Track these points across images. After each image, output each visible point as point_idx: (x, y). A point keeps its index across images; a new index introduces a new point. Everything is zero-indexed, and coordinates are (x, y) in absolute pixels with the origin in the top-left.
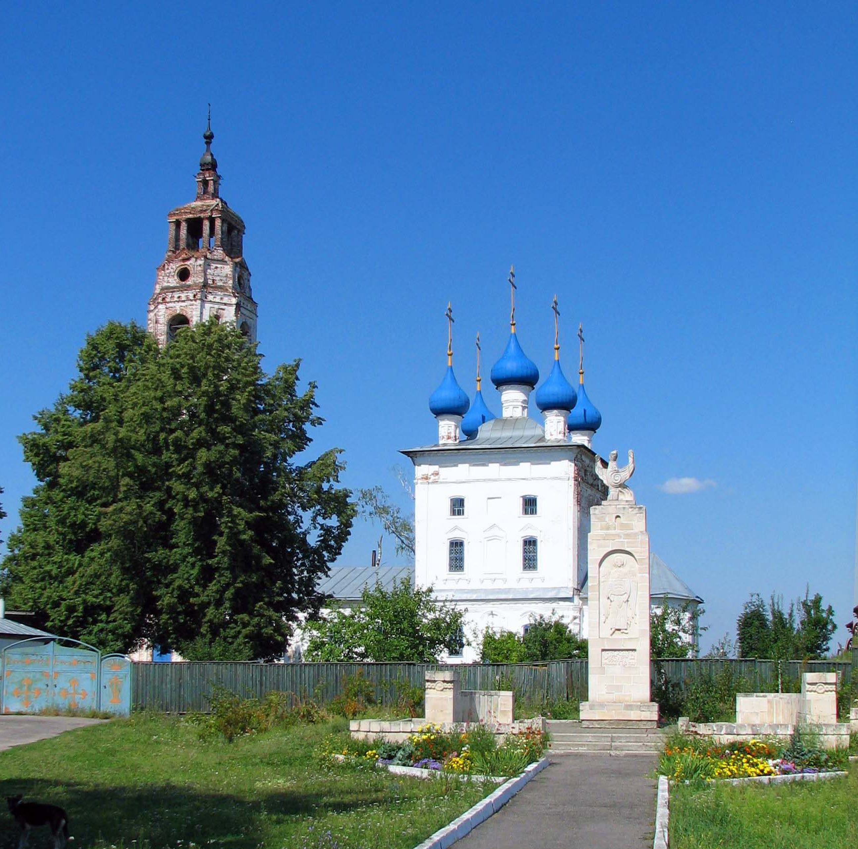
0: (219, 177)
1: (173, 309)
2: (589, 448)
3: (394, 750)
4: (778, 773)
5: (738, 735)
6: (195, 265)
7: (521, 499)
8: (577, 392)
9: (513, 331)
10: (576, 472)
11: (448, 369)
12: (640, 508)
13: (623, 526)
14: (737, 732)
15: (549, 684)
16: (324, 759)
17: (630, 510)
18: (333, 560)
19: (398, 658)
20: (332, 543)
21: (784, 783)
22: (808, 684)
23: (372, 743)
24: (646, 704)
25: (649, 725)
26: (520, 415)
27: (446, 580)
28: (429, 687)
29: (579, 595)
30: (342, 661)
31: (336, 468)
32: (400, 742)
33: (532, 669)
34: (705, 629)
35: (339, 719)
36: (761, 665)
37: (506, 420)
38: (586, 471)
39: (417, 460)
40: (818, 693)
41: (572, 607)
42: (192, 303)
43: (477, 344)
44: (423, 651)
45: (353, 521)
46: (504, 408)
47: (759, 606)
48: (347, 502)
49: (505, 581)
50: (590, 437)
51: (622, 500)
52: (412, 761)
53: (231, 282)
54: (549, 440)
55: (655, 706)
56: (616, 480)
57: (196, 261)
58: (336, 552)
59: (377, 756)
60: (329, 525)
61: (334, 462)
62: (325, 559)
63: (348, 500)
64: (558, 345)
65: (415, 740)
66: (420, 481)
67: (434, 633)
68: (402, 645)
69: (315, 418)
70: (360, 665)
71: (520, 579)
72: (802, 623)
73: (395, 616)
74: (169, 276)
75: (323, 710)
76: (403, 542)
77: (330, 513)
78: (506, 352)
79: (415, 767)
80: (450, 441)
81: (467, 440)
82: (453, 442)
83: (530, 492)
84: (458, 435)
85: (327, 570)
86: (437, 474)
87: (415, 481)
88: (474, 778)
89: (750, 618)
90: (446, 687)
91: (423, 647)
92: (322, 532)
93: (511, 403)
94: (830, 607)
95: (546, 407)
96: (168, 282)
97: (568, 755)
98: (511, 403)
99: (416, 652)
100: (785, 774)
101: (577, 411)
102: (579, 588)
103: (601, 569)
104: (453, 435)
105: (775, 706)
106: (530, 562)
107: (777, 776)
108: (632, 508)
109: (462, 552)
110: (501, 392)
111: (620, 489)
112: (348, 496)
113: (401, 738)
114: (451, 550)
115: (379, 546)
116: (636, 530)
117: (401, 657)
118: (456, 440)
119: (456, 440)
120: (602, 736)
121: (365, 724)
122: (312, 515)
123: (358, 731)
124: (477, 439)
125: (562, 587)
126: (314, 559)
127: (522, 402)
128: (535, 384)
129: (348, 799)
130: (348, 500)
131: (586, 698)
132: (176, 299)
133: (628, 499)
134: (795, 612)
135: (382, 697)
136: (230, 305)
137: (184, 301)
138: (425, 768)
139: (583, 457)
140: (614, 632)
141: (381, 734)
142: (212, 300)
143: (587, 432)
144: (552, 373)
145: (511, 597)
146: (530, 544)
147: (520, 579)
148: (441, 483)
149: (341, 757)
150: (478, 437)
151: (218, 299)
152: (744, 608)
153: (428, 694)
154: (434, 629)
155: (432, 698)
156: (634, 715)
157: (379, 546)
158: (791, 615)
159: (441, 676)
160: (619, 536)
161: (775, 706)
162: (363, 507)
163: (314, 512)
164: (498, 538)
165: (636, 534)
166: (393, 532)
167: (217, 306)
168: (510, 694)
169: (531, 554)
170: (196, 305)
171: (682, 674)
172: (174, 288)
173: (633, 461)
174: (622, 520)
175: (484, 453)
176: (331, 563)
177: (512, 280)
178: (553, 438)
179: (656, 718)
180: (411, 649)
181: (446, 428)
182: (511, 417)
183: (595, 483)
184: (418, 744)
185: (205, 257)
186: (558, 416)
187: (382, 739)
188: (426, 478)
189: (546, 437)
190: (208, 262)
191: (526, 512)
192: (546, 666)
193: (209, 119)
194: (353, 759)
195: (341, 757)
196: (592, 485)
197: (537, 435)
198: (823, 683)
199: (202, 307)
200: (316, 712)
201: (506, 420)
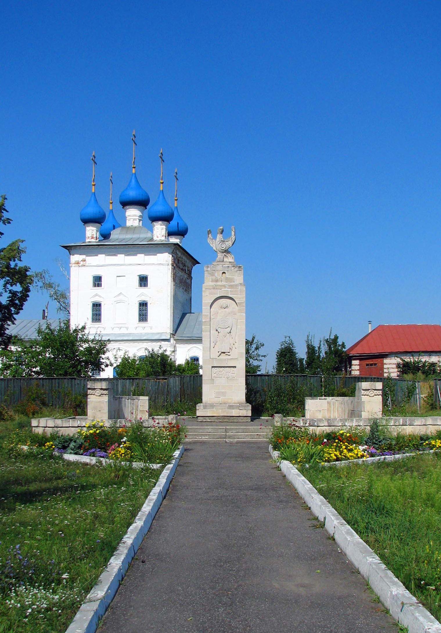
3: (67, 442)
4: (368, 456)
5: (318, 426)
7: (138, 277)
8: (174, 210)
9: (134, 172)
10: (173, 261)
11: (92, 194)
12: (240, 267)
13: (227, 280)
14: (317, 424)
15: (168, 391)
16: (12, 449)
17: (233, 268)
18: (17, 313)
19: (64, 375)
20: (17, 302)
21: (373, 463)
22: (363, 390)
23: (50, 436)
24: (243, 405)
25: (245, 420)
26: (138, 225)
27: (90, 328)
28: (90, 393)
29: (174, 338)
30: (24, 377)
31: (19, 251)
32: (71, 435)
34: (264, 356)
35: (24, 418)
36: (311, 379)
37: (128, 228)
38: (178, 260)
39: (72, 252)
40: (370, 396)
41: (169, 345)
43: (111, 180)
44: (80, 370)
45: (31, 287)
46: (127, 220)
47: (290, 344)
48: (27, 275)
49: (127, 328)
50: (181, 240)
51: (226, 262)
52: (82, 451)
54: (156, 240)
55: (250, 407)
56: (222, 248)
58: (19, 308)
59: (54, 447)
60: (15, 290)
61: (18, 248)
62: (13, 312)
63: (28, 273)
64: (163, 181)
65: (84, 434)
66: (73, 265)
67: (88, 357)
68: (66, 366)
69: (6, 219)
70: (37, 379)
72: (326, 353)
73: (61, 346)
75: (11, 411)
76: (61, 305)
77: (16, 282)
78: (129, 185)
79: (85, 455)
80: (93, 240)
81: (103, 240)
82: (94, 241)
83: (143, 273)
84: (98, 236)
85: (13, 320)
86: (85, 261)
87: (70, 265)
88: (135, 465)
89: (284, 352)
90: (103, 393)
91: (81, 367)
92: (10, 295)
93: (131, 218)
94: (343, 343)
95: (155, 219)
97: (195, 443)
98: (131, 218)
99: (76, 370)
100: (373, 457)
101: (173, 223)
102: (174, 333)
103: (211, 309)
104: (95, 236)
105: (332, 406)
106: (143, 317)
107: (368, 459)
108: (233, 267)
109: (100, 310)
111: (225, 253)
112: (27, 271)
113: (71, 432)
115: (47, 308)
116: (237, 282)
117: (66, 374)
119: (97, 239)
120: (219, 428)
121: (43, 422)
122: (3, 283)
123: (37, 426)
126: (5, 313)
127: (139, 217)
128: (147, 206)
129: (33, 487)
130: (28, 273)
131: (201, 401)
133: (230, 261)
134: (322, 345)
135: (53, 401)
138: (93, 456)
141: (55, 429)
143: (179, 237)
144: (159, 198)
145: (131, 339)
148: (87, 266)
149: (25, 448)
150: (111, 237)
152: (280, 345)
153: (89, 398)
154: (88, 355)
155: (93, 401)
156: (235, 412)
157: (47, 308)
158: (319, 348)
159: (98, 385)
160: (224, 286)
161: (332, 406)
162: (36, 283)
163: (5, 281)
164: (124, 302)
165: (236, 285)
166: (55, 299)
168: (147, 398)
169: (144, 312)
171: (258, 385)
173: (235, 235)
174: (227, 275)
175: (116, 248)
176: (16, 315)
177: (134, 139)
178: (158, 239)
179: (250, 414)
180: (72, 369)
181: (91, 232)
182: (132, 226)
183: (184, 268)
184: (86, 437)
186: (162, 225)
187: (57, 433)
189: (154, 238)
191: (141, 285)
194: (35, 449)
195: (25, 448)
196: (182, 269)
198: (373, 389)
200: (6, 412)
201: (128, 227)
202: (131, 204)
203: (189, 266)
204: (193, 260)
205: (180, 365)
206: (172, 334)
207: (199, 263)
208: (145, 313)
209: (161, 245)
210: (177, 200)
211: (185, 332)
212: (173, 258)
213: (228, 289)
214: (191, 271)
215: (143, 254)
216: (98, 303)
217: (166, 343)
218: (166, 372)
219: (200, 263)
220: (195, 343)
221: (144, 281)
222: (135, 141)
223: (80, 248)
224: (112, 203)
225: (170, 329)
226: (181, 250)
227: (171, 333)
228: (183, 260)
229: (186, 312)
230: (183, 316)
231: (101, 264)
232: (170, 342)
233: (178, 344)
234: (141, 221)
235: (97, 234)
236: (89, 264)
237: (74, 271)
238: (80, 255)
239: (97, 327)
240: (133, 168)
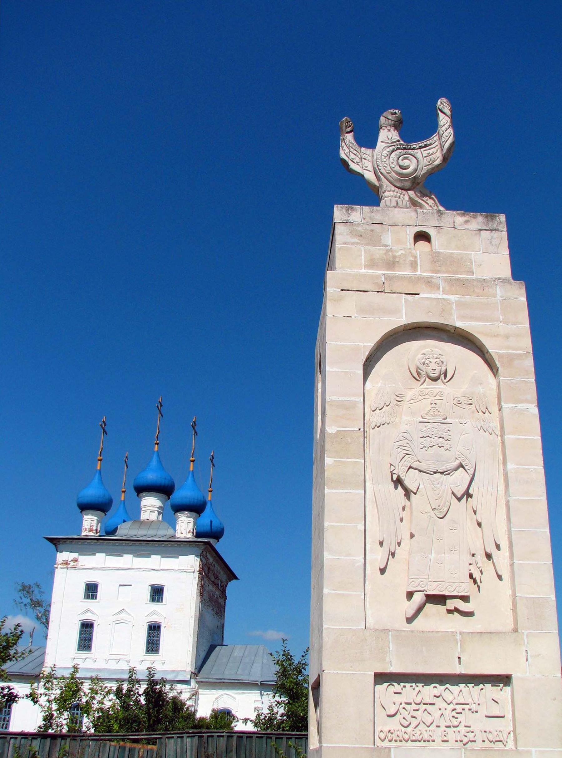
7: (150, 587)
27: (74, 659)
33: (124, 748)
37: (143, 522)
38: (209, 568)
39: (60, 547)
46: (142, 512)
54: (179, 538)
56: (401, 167)
64: (194, 459)
66: (60, 566)
71: (142, 661)
80: (91, 534)
83: (158, 581)
84: (99, 529)
87: (56, 566)
95: (179, 508)
102: (196, 673)
103: (368, 383)
104: (94, 528)
109: (91, 634)
111: (411, 193)
118: (97, 533)
124: (116, 534)
125: (180, 671)
139: (208, 554)
140: (420, 609)
146: (154, 630)
147: (142, 661)
164: (126, 622)
169: (155, 639)
181: (89, 521)
182: (148, 519)
188: (66, 563)
189: (176, 536)
192: (154, 743)
196: (213, 582)
197: (168, 535)
203: (224, 580)
205: (202, 719)
206: (193, 673)
208: (156, 640)
209: (186, 543)
210: (211, 491)
211: (212, 672)
213: (445, 297)
214: (226, 589)
215: (160, 555)
216: (89, 623)
218: (159, 721)
219: (238, 578)
220: (228, 689)
221: (158, 594)
222: (161, 411)
223: (71, 543)
224: (124, 492)
225: (191, 665)
226: (214, 554)
228: (216, 569)
229: (216, 643)
230: (212, 649)
231: (99, 566)
232: (190, 685)
234: (161, 515)
235: (97, 525)
236: (81, 566)
238: (71, 552)
239: (85, 657)
240: (156, 444)
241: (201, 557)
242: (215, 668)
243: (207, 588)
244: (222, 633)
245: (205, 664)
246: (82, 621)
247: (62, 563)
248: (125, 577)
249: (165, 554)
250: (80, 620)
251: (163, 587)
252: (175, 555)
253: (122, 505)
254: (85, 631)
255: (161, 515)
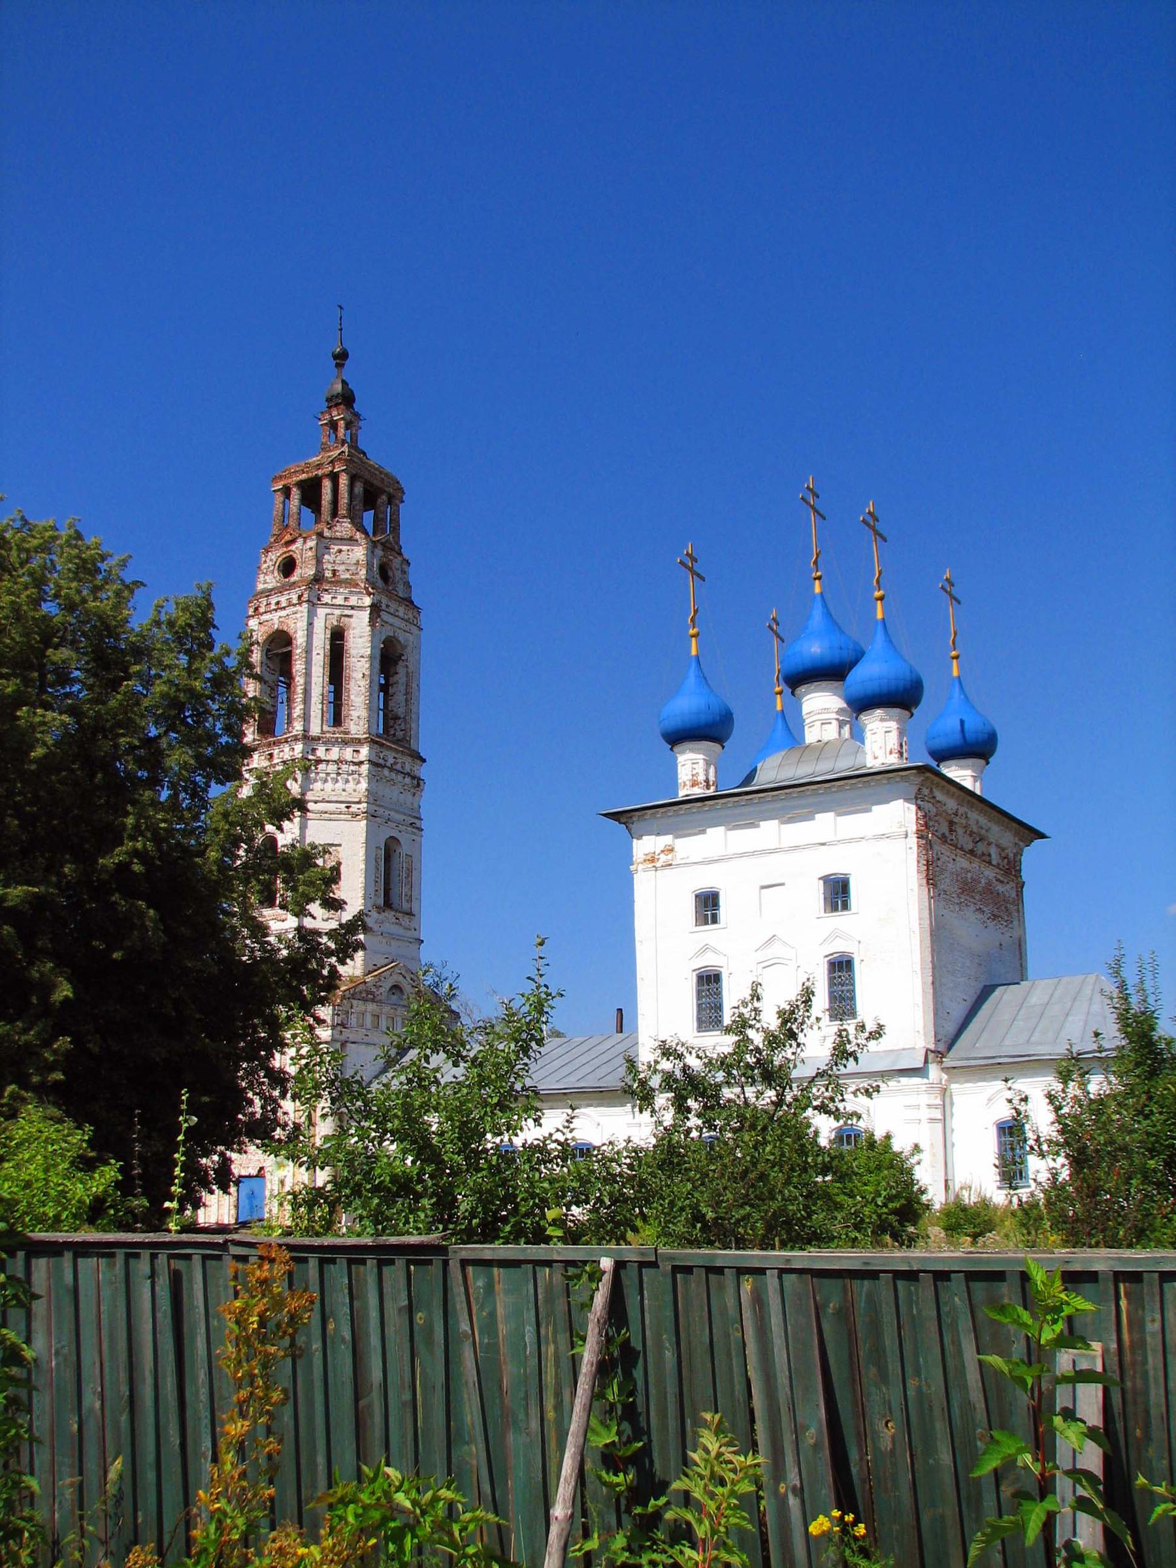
0: (357, 415)
1: (270, 623)
2: (978, 792)
6: (304, 550)
7: (821, 882)
9: (817, 589)
38: (951, 823)
41: (924, 1087)
42: (295, 609)
46: (806, 728)
53: (364, 572)
54: (871, 768)
57: (305, 542)
64: (881, 593)
66: (641, 867)
74: (266, 574)
83: (836, 868)
84: (712, 778)
86: (672, 850)
96: (265, 582)
104: (702, 778)
110: (800, 699)
114: (699, 992)
118: (708, 787)
125: (904, 1049)
127: (837, 713)
132: (273, 607)
136: (361, 608)
137: (284, 608)
142: (330, 602)
143: (970, 761)
151: (340, 600)
164: (783, 961)
167: (337, 612)
170: (302, 612)
172: (272, 590)
181: (689, 765)
182: (819, 741)
185: (320, 535)
190: (324, 543)
193: (341, 330)
196: (972, 852)
199: (311, 615)
202: (805, 679)
204: (1014, 825)
206: (932, 1051)
207: (1042, 836)
212: (920, 814)
216: (712, 973)
217: (916, 1080)
219: (1048, 835)
225: (925, 1034)
227: (927, 1050)
233: (956, 1083)
234: (848, 726)
235: (707, 771)
237: (644, 884)
238: (658, 834)
241: (919, 802)
242: (985, 1035)
243: (950, 865)
244: (1018, 956)
245: (966, 1028)
246: (698, 972)
247: (645, 861)
248: (769, 869)
249: (843, 808)
250: (694, 970)
251: (848, 879)
252: (863, 805)
253: (780, 721)
254: (708, 990)
255: (848, 726)
